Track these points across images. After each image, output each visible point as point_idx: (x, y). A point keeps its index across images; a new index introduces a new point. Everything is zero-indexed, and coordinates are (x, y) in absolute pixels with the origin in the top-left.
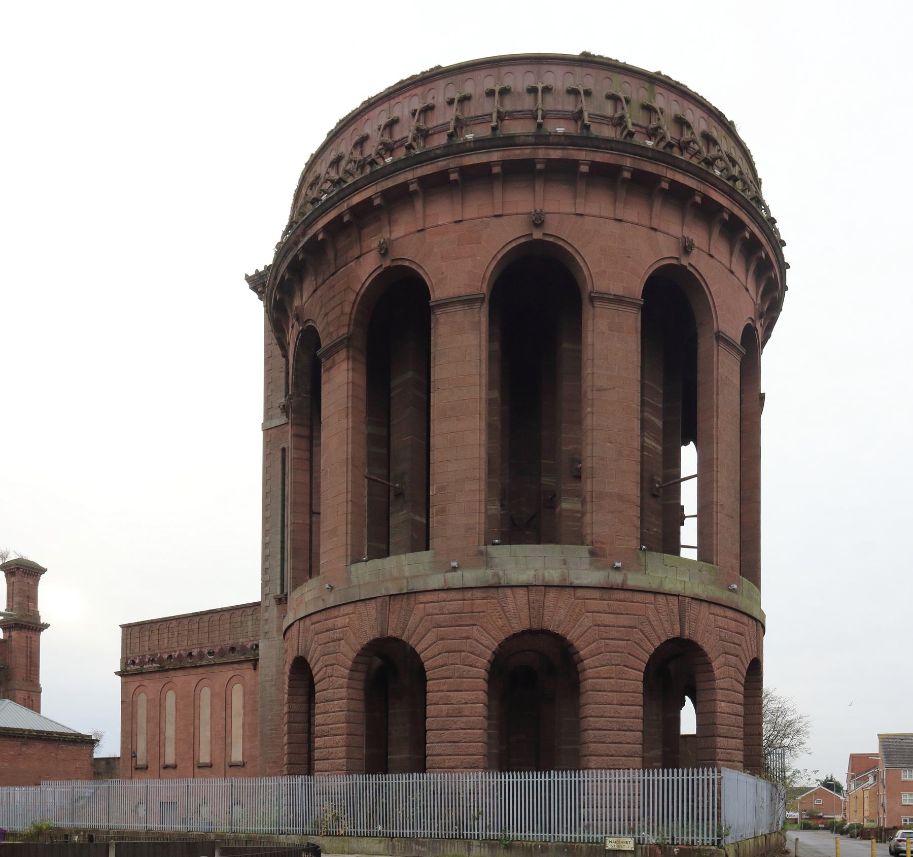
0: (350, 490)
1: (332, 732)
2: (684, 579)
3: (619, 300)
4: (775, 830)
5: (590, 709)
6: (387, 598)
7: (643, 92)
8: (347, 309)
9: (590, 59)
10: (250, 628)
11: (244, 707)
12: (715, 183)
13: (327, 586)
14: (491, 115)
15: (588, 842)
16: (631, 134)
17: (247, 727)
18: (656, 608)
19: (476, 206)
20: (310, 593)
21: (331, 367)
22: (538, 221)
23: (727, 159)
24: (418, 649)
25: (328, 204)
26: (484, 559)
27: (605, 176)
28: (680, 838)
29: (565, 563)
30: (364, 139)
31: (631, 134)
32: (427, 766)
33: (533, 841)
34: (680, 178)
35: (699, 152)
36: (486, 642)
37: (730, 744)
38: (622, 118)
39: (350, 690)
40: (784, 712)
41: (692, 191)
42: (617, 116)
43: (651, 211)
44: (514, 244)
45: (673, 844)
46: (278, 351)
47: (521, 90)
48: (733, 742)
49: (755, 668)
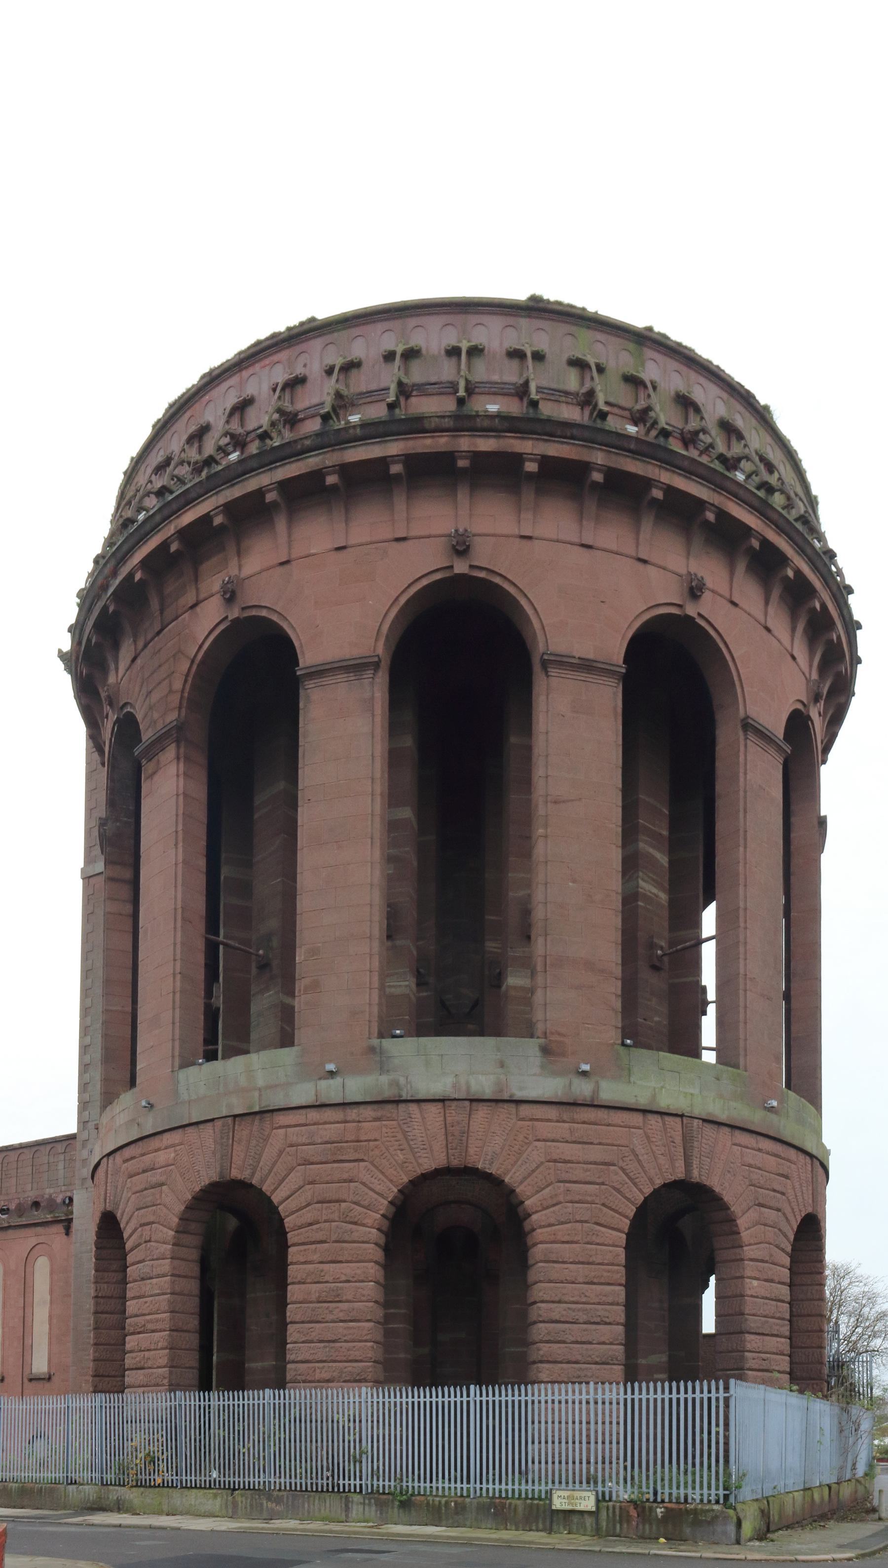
0: (178, 957)
1: (150, 1326)
2: (692, 1091)
3: (586, 666)
4: (848, 1476)
5: (539, 1291)
6: (230, 1120)
7: (625, 357)
8: (178, 685)
9: (541, 305)
10: (61, 1172)
11: (51, 1292)
12: (736, 492)
13: (144, 1103)
14: (388, 389)
15: (527, 1498)
16: (603, 416)
17: (55, 1321)
18: (645, 1132)
19: (368, 524)
20: (122, 1115)
21: (154, 773)
22: (461, 547)
23: (757, 459)
24: (275, 1199)
25: (148, 527)
26: (377, 1059)
27: (563, 479)
28: (667, 1491)
29: (502, 1065)
30: (203, 430)
31: (603, 416)
32: (288, 1378)
33: (444, 1496)
34: (680, 483)
35: (712, 446)
36: (378, 1188)
37: (769, 1345)
38: (591, 393)
39: (176, 1262)
40: (872, 1298)
41: (701, 504)
42: (584, 390)
43: (638, 533)
44: (425, 582)
45: (655, 1501)
46: (96, 756)
47: (436, 353)
48: (773, 1343)
49: (810, 1231)
